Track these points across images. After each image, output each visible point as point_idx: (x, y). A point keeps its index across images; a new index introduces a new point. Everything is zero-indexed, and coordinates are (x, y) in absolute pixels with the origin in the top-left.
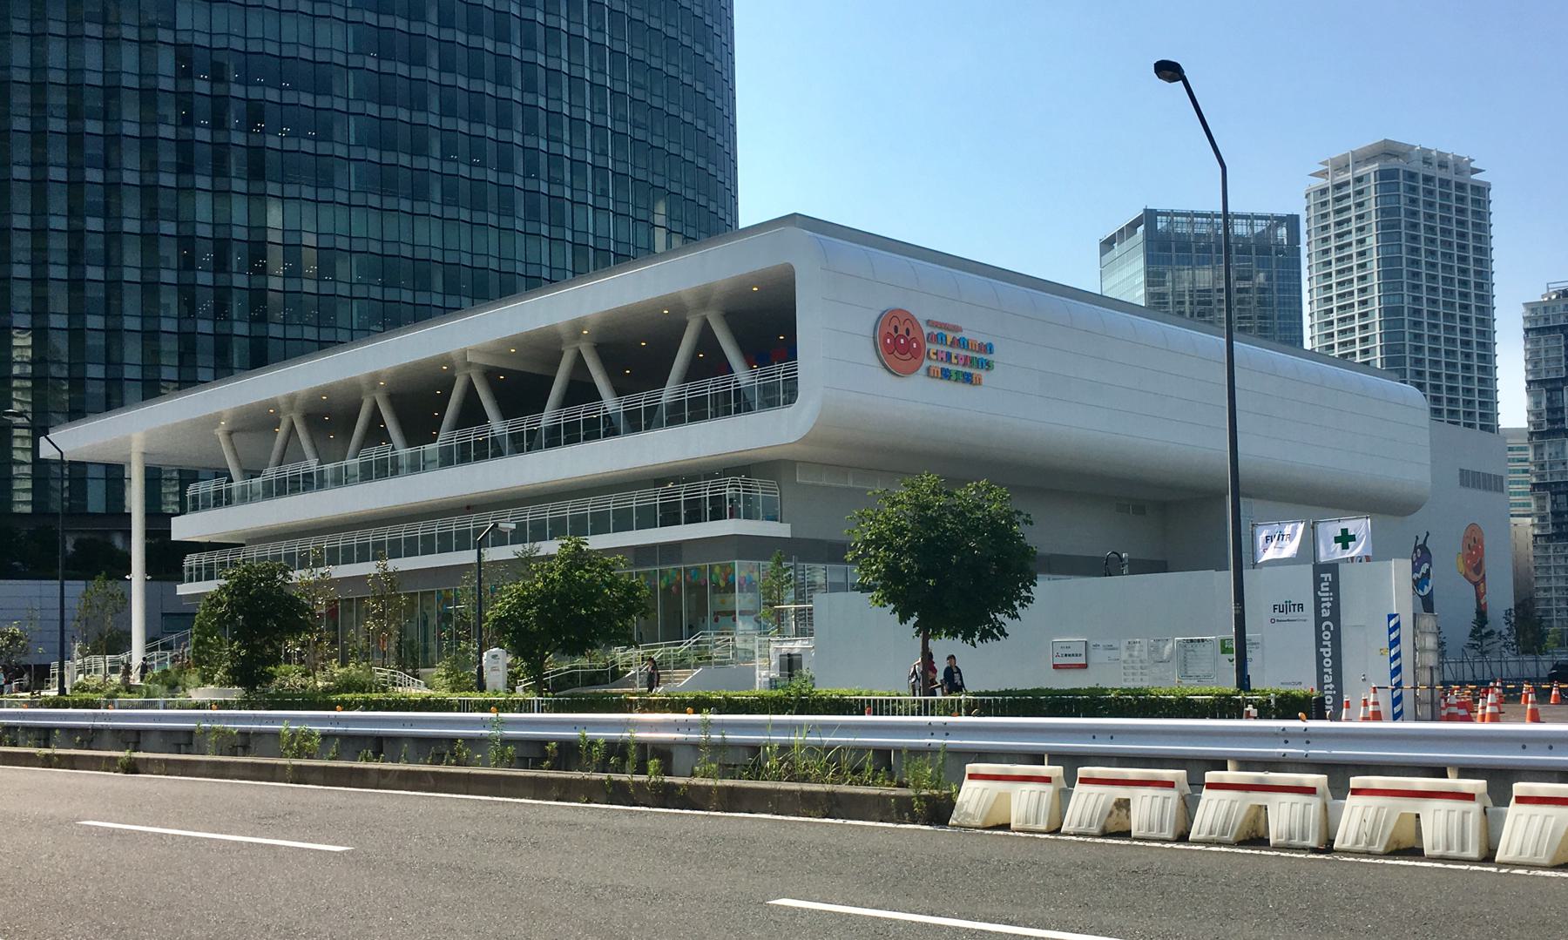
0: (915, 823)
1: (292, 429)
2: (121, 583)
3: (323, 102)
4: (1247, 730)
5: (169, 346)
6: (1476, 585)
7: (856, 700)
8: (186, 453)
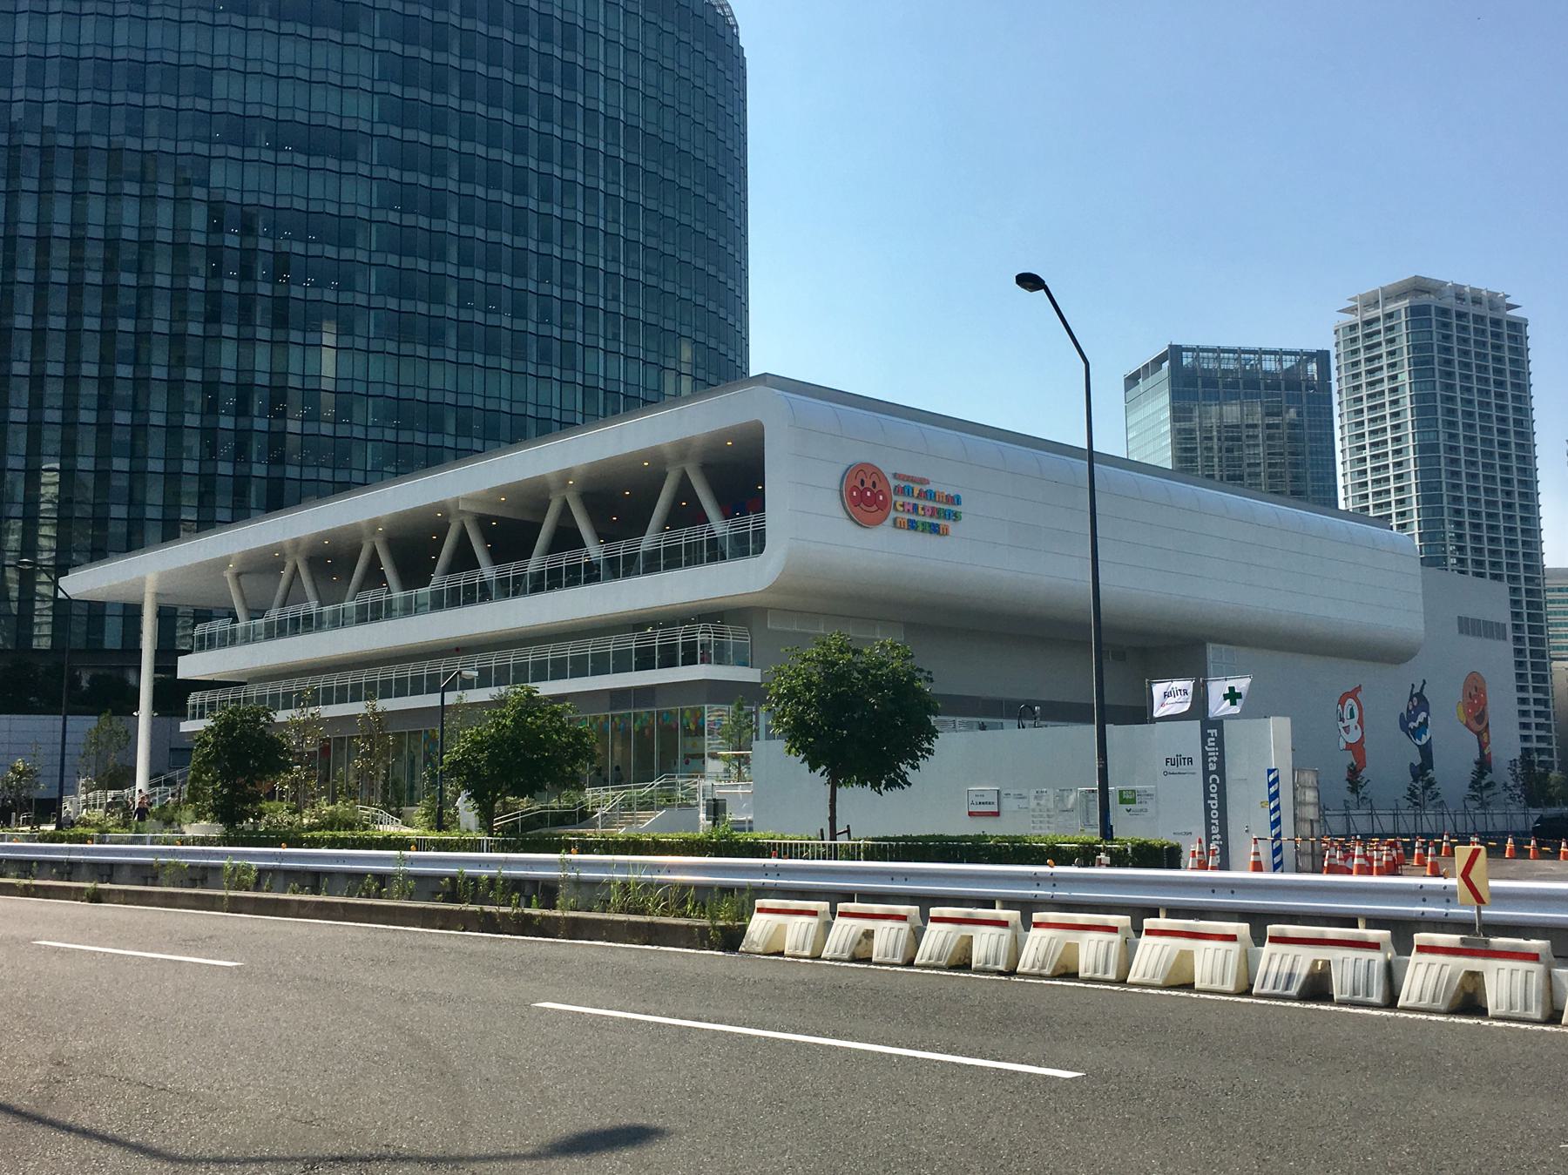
0: (712, 949)
1: (296, 571)
2: (130, 718)
3: (347, 254)
4: (1187, 880)
5: (191, 487)
6: (1479, 734)
7: (769, 843)
8: (192, 594)
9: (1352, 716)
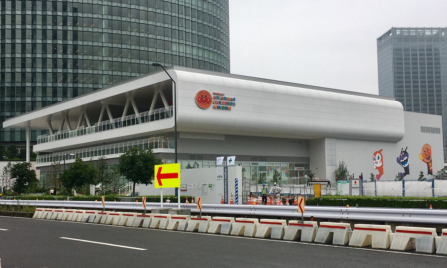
6: (428, 163)
9: (379, 158)
